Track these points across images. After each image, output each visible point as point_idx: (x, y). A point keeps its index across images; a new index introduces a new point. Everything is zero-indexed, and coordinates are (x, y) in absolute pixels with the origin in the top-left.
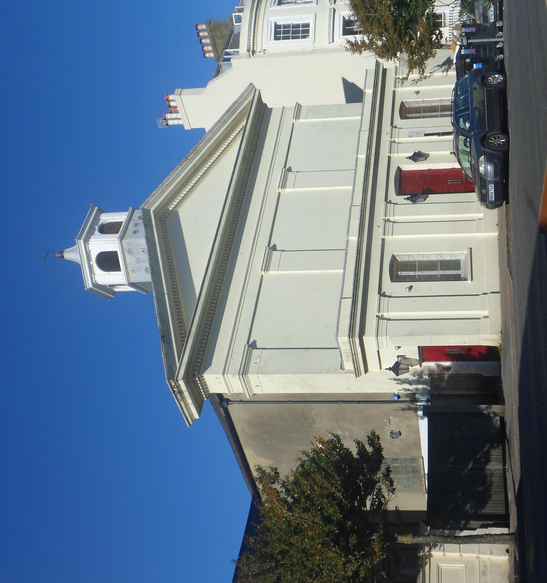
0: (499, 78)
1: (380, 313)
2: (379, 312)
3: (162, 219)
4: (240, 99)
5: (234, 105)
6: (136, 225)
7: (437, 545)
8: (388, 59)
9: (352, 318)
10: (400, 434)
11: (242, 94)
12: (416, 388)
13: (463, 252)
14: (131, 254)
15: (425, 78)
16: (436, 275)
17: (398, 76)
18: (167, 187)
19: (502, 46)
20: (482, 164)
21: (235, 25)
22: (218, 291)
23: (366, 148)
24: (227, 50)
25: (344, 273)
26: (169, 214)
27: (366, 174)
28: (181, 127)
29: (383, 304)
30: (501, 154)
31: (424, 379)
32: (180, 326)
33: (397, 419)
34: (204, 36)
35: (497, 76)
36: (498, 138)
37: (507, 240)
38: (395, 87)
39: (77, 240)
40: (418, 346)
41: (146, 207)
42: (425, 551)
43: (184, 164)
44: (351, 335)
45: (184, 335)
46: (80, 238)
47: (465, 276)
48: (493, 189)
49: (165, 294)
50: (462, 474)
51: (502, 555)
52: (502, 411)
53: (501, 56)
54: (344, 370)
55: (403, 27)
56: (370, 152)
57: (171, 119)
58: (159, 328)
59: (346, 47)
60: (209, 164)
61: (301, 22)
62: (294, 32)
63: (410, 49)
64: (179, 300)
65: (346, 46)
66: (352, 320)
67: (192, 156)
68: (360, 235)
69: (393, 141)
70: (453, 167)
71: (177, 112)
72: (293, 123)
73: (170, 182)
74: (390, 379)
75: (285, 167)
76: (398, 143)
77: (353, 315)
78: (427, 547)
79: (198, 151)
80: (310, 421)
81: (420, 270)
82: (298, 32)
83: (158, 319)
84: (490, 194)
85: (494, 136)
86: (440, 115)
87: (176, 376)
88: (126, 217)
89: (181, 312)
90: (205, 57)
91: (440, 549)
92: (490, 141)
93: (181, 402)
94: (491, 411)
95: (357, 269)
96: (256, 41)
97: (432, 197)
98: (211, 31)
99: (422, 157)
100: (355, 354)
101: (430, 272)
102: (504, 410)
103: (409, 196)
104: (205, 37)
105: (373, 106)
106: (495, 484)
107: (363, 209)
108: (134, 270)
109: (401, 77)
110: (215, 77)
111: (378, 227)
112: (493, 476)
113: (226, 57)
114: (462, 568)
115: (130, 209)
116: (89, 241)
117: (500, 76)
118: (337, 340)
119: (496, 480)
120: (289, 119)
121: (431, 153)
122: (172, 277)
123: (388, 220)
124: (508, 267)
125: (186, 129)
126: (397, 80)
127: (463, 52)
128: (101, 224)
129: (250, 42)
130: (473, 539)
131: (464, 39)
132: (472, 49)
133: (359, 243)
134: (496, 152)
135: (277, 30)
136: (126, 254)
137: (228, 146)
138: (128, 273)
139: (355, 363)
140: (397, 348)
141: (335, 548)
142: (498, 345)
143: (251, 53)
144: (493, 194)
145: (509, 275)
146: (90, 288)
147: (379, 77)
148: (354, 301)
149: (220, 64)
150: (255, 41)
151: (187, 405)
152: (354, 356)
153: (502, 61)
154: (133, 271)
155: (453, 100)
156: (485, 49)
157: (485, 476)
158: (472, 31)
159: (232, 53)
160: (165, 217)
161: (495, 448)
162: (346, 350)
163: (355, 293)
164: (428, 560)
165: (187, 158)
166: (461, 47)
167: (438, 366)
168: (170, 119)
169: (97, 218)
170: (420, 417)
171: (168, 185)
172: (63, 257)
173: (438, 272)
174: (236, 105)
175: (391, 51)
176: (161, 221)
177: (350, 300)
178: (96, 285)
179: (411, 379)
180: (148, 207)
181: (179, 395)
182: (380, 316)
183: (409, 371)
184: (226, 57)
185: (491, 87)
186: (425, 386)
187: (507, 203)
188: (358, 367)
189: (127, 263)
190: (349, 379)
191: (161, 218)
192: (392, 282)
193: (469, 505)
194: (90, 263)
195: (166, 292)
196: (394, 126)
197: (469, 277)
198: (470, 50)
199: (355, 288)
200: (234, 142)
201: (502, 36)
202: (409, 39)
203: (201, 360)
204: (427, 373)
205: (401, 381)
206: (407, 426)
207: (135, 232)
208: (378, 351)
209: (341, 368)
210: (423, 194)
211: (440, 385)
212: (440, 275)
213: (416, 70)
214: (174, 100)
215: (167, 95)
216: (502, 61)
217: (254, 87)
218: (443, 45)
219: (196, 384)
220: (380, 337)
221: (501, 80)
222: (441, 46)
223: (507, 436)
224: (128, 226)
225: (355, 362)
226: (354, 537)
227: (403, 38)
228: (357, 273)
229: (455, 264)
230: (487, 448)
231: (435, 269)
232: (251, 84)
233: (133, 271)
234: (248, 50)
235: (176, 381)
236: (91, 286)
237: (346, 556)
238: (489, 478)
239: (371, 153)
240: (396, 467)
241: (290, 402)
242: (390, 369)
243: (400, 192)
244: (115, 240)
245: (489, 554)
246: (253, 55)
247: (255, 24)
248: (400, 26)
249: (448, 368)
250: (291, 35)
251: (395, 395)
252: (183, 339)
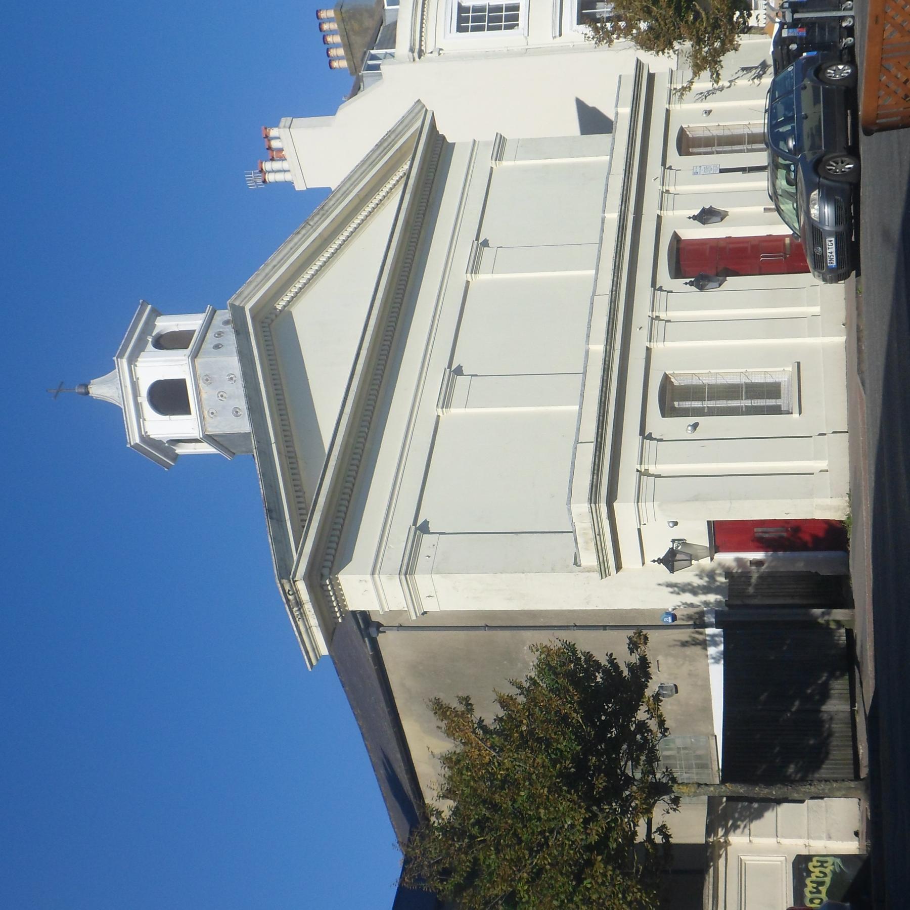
1: (642, 466)
2: (641, 464)
3: (264, 325)
5: (389, 136)
6: (219, 334)
7: (739, 827)
8: (657, 53)
9: (595, 472)
10: (677, 692)
11: (404, 118)
12: (705, 601)
14: (211, 383)
15: (721, 89)
16: (739, 407)
19: (851, 23)
20: (815, 204)
21: (389, 10)
22: (362, 440)
23: (618, 202)
24: (373, 52)
27: (619, 243)
28: (289, 185)
29: (647, 453)
30: (847, 187)
31: (718, 584)
33: (671, 660)
34: (331, 31)
35: (841, 67)
36: (842, 163)
38: (669, 104)
39: (117, 358)
41: (237, 303)
42: (718, 836)
43: (303, 232)
44: (593, 497)
45: (304, 511)
46: (121, 356)
48: (834, 246)
51: (847, 840)
52: (850, 619)
53: (850, 40)
54: (580, 566)
56: (625, 207)
57: (273, 171)
58: (263, 497)
59: (586, 34)
60: (346, 234)
62: (491, 20)
67: (316, 219)
68: (609, 340)
69: (666, 190)
70: (769, 234)
71: (283, 159)
73: (279, 263)
74: (660, 585)
75: (477, 239)
76: (669, 292)
77: (596, 467)
78: (722, 830)
79: (327, 211)
80: (520, 665)
81: (710, 399)
82: (499, 19)
83: (260, 482)
84: (828, 254)
85: (835, 160)
88: (201, 322)
89: (298, 474)
90: (331, 67)
92: (829, 168)
93: (299, 623)
94: (831, 618)
95: (603, 395)
97: (732, 281)
98: (343, 20)
99: (717, 216)
100: (599, 535)
101: (729, 402)
102: (853, 616)
103: (693, 279)
104: (332, 32)
105: (631, 133)
106: (837, 735)
108: (215, 412)
109: (679, 87)
110: (350, 98)
111: (640, 329)
113: (370, 62)
114: (779, 863)
115: (209, 308)
117: (846, 68)
118: (569, 510)
119: (839, 728)
120: (484, 160)
123: (647, 473)
124: (859, 374)
127: (785, 33)
129: (414, 36)
132: (800, 29)
133: (608, 354)
134: (837, 184)
135: (462, 25)
137: (377, 204)
138: (204, 417)
139: (600, 551)
140: (671, 525)
142: (844, 518)
143: (416, 55)
144: (834, 254)
146: (137, 443)
147: (639, 107)
148: (598, 446)
149: (360, 74)
150: (423, 34)
151: (308, 629)
152: (598, 537)
153: (851, 49)
154: (212, 413)
155: (767, 108)
156: (822, 28)
157: (821, 722)
159: (382, 57)
160: (269, 321)
161: (837, 678)
162: (585, 529)
163: (600, 433)
164: (723, 849)
165: (307, 223)
168: (269, 172)
169: (149, 324)
171: (274, 266)
173: (742, 402)
174: (393, 137)
175: (664, 37)
177: (592, 447)
178: (146, 439)
179: (695, 585)
181: (297, 609)
182: (643, 470)
184: (370, 62)
186: (719, 597)
188: (605, 559)
189: (203, 399)
190: (588, 583)
191: (263, 322)
192: (663, 416)
194: (137, 399)
196: (657, 287)
197: (796, 409)
199: (600, 425)
201: (852, 7)
202: (693, 18)
203: (334, 550)
206: (689, 674)
207: (217, 347)
208: (639, 530)
209: (576, 563)
211: (747, 589)
212: (746, 406)
213: (706, 74)
214: (278, 138)
215: (266, 128)
216: (851, 49)
217: (424, 106)
218: (752, 27)
219: (326, 591)
220: (643, 504)
221: (847, 73)
222: (748, 30)
223: (857, 658)
224: (205, 337)
225: (600, 550)
226: (601, 778)
229: (773, 390)
230: (824, 678)
231: (738, 398)
233: (212, 413)
234: (412, 50)
235: (292, 582)
236: (138, 441)
237: (588, 809)
239: (628, 209)
240: (668, 756)
241: (487, 627)
242: (660, 561)
243: (677, 272)
244: (182, 360)
245: (825, 838)
246: (420, 58)
249: (759, 563)
250: (486, 23)
252: (303, 517)
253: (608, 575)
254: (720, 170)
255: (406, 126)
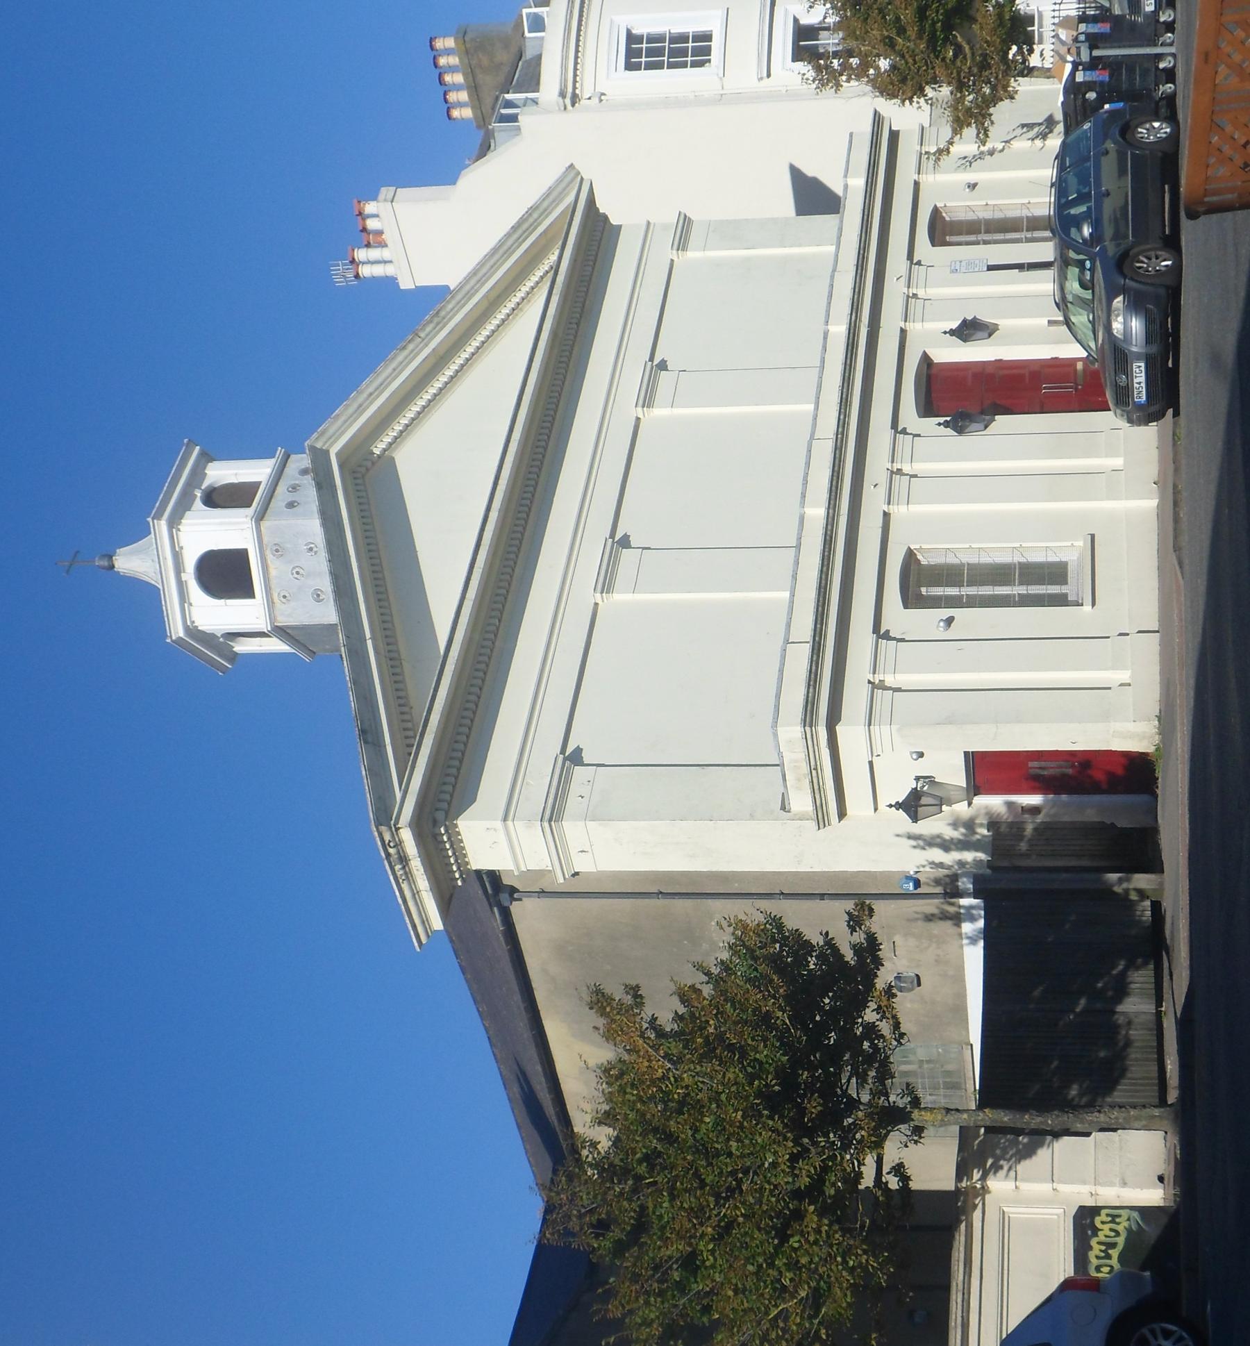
0: (1162, 129)
2: (874, 673)
4: (544, 200)
6: (294, 488)
7: (1001, 1167)
9: (812, 683)
10: (919, 984)
11: (550, 191)
12: (960, 860)
13: (1076, 544)
14: (282, 555)
15: (991, 153)
17: (925, 148)
18: (370, 399)
19: (1172, 65)
20: (1117, 316)
21: (530, 38)
25: (792, 602)
26: (373, 464)
28: (391, 281)
30: (1162, 291)
32: (402, 713)
33: (912, 942)
34: (450, 67)
35: (1156, 125)
36: (1157, 258)
37: (1174, 493)
38: (919, 174)
39: (153, 519)
40: (965, 752)
41: (319, 445)
43: (411, 347)
45: (410, 733)
46: (158, 516)
47: (1078, 598)
48: (1143, 374)
49: (366, 640)
50: (1061, 1023)
53: (1169, 87)
54: (789, 812)
55: (939, 24)
58: (354, 713)
59: (804, 74)
61: (690, 28)
62: (673, 53)
63: (955, 75)
64: (399, 654)
65: (802, 72)
66: (811, 687)
67: (428, 329)
68: (832, 502)
71: (383, 245)
72: (672, 260)
73: (377, 389)
74: (898, 836)
75: (652, 359)
78: (978, 1172)
82: (683, 52)
83: (351, 693)
84: (1135, 385)
86: (1026, 238)
87: (394, 818)
88: (269, 471)
89: (402, 682)
91: (1007, 1175)
92: (1138, 265)
93: (402, 885)
94: (1131, 886)
96: (582, 73)
97: (1003, 422)
98: (467, 52)
100: (816, 769)
101: (997, 588)
102: (1161, 884)
103: (948, 419)
104: (452, 69)
105: (866, 213)
107: (839, 444)
109: (933, 149)
110: (477, 160)
111: (875, 486)
112: (1133, 1027)
113: (504, 111)
114: (1056, 1217)
115: (280, 452)
116: (180, 523)
117: (1164, 126)
118: (775, 735)
119: (1140, 1035)
120: (662, 251)
121: (1002, 323)
122: (382, 603)
125: (402, 287)
126: (924, 157)
127: (1080, 77)
128: (209, 486)
130: (1081, 1116)
131: (1082, 48)
132: (1101, 72)
133: (830, 520)
134: (1150, 289)
136: (270, 557)
137: (514, 309)
138: (273, 603)
139: (816, 791)
140: (915, 756)
141: (774, 1120)
142: (1150, 749)
143: (568, 101)
144: (1143, 385)
145: (1177, 568)
147: (880, 148)
150: (578, 73)
151: (416, 894)
152: (814, 772)
153: (1171, 99)
154: (285, 597)
155: (1054, 180)
156: (1131, 70)
157: (1115, 1028)
158: (1102, 30)
161: (1138, 968)
163: (818, 630)
164: (980, 1198)
165: (417, 334)
166: (1076, 66)
167: (1010, 805)
169: (198, 474)
170: (968, 938)
171: (371, 394)
172: (113, 567)
174: (535, 215)
176: (355, 478)
177: (807, 648)
178: (192, 631)
180: (324, 445)
181: (400, 866)
182: (877, 682)
183: (941, 811)
184: (504, 111)
185: (1144, 149)
187: (1176, 414)
188: (824, 802)
191: (354, 472)
192: (906, 607)
193: (1075, 1087)
195: (368, 634)
198: (1097, 72)
199: (819, 619)
200: (529, 301)
201: (1173, 42)
203: (465, 737)
204: (985, 822)
205: (925, 840)
207: (291, 505)
209: (783, 808)
210: (982, 413)
213: (970, 132)
214: (377, 216)
215: (359, 202)
216: (1171, 99)
217: (579, 173)
218: (1034, 67)
220: (877, 727)
221: (1166, 133)
222: (1028, 71)
224: (274, 492)
225: (816, 790)
227: (940, 51)
228: (823, 585)
229: (1056, 573)
230: (1121, 967)
232: (572, 166)
233: (285, 597)
234: (562, 94)
235: (393, 829)
236: (181, 634)
237: (796, 1142)
238: (1123, 1032)
239: (860, 320)
242: (898, 806)
243: (927, 408)
244: (243, 523)
246: (573, 105)
247: (579, 30)
248: (934, 23)
249: (1035, 810)
250: (666, 58)
251: (909, 878)
253: (821, 826)
254: (988, 266)
255: (553, 201)
